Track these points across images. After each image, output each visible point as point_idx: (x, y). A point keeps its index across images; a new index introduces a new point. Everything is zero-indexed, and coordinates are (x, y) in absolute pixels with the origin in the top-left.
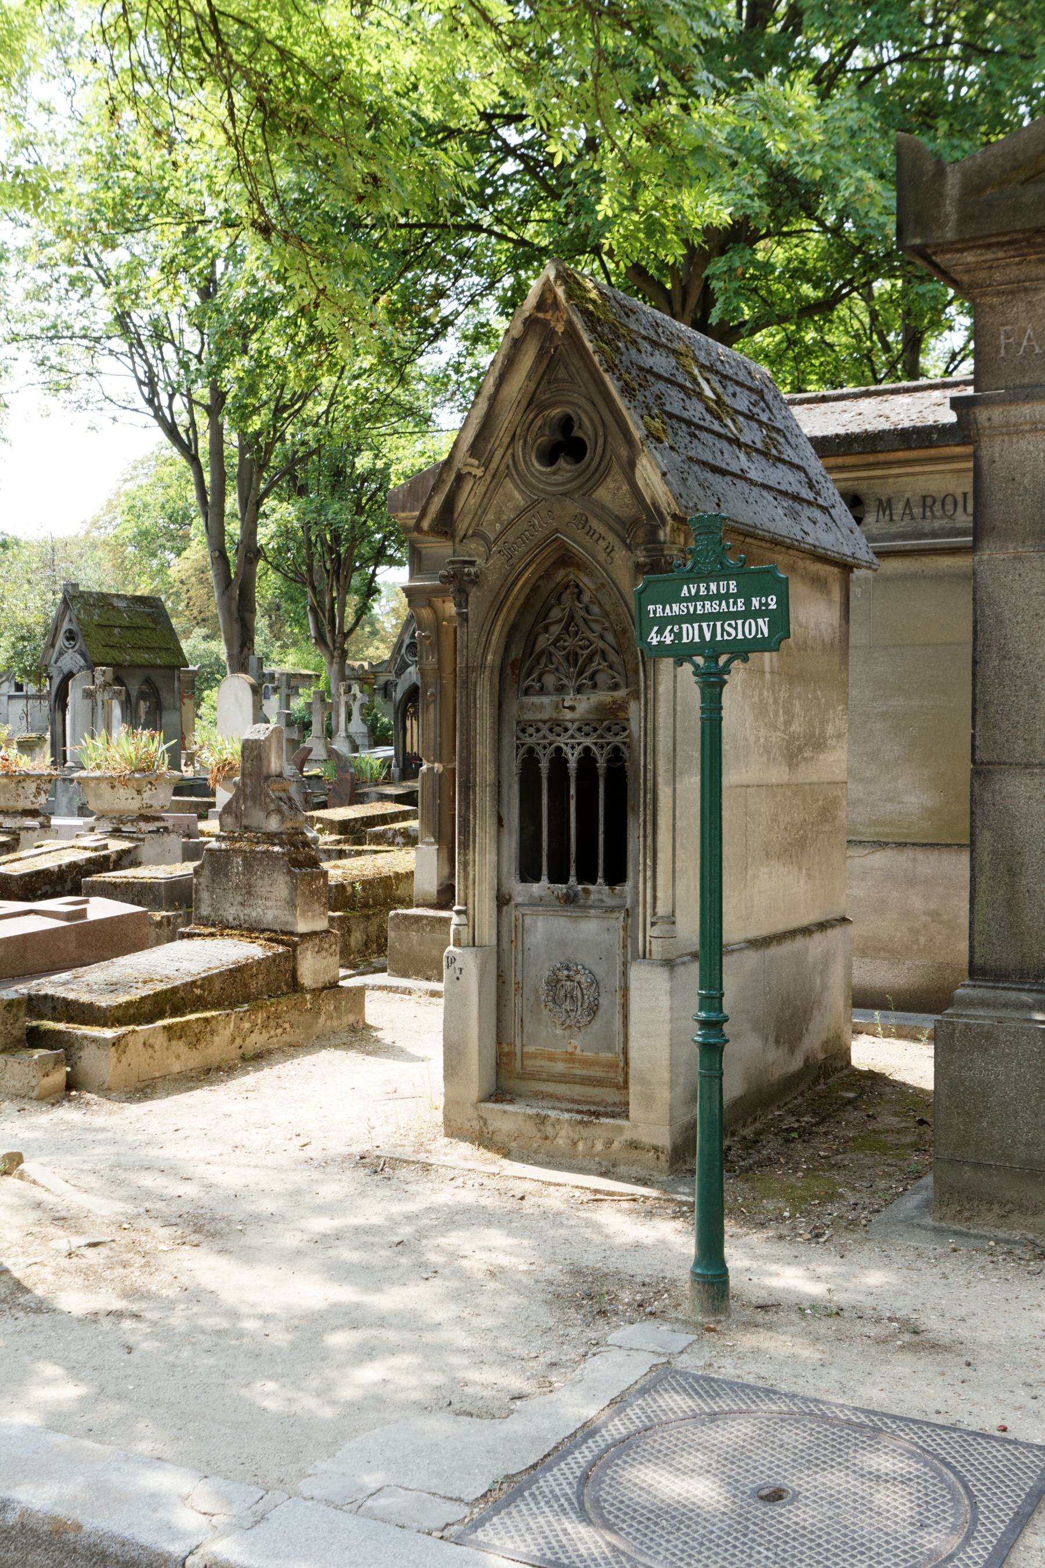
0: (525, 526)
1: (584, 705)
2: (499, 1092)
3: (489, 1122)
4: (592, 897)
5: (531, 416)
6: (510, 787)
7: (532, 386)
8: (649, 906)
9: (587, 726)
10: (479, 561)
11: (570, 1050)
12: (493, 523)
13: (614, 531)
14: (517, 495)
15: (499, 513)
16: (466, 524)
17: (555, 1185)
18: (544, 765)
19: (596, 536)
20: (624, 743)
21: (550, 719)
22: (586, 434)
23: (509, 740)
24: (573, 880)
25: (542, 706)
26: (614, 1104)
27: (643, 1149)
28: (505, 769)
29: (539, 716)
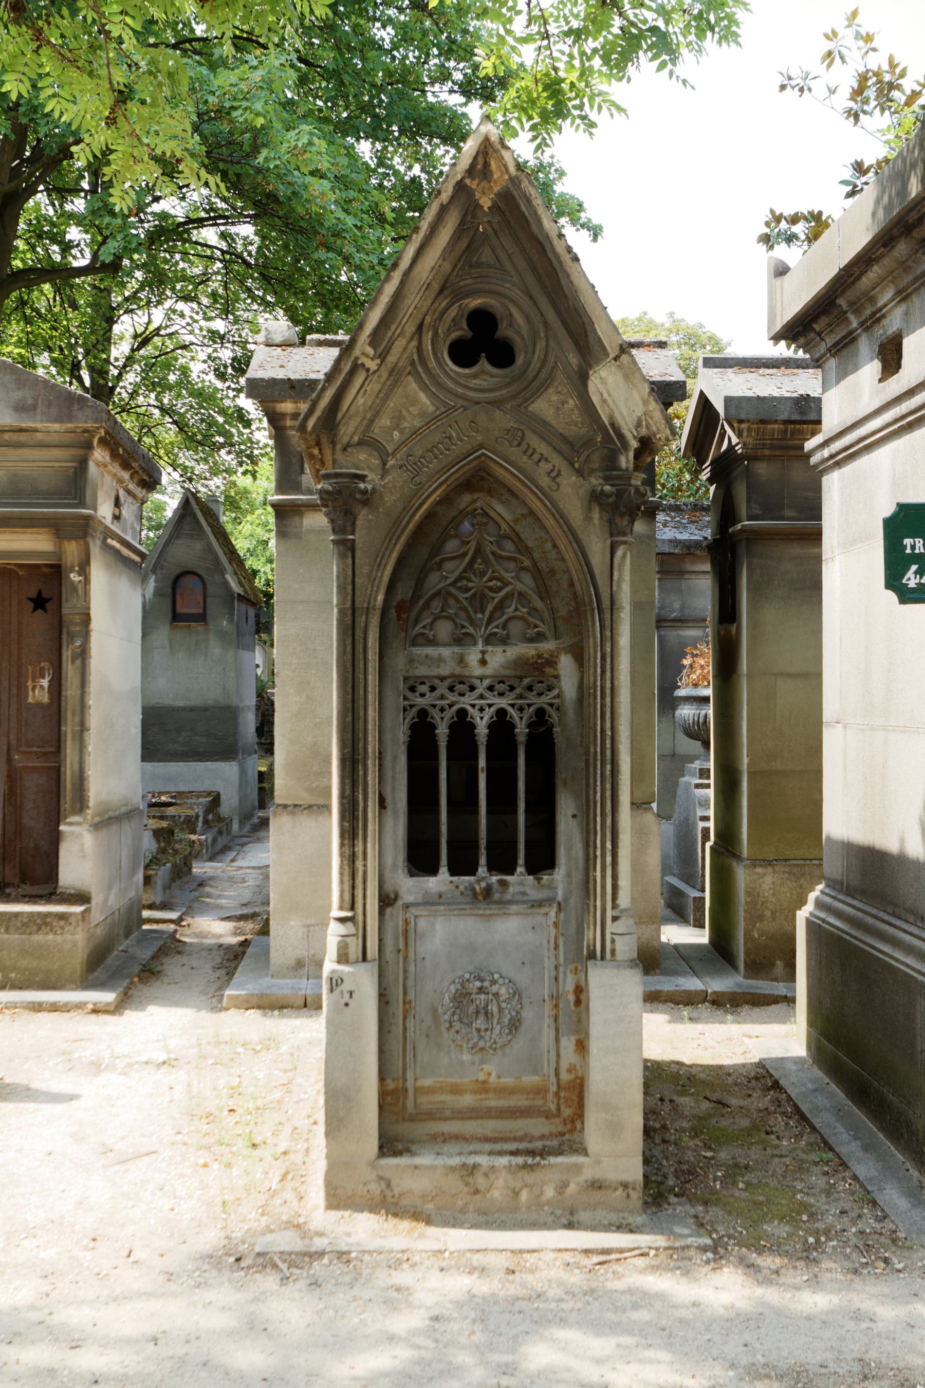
0: (438, 437)
1: (499, 659)
2: (390, 1145)
3: (394, 1183)
4: (511, 890)
5: (444, 304)
6: (395, 758)
7: (447, 267)
10: (371, 476)
11: (482, 1077)
12: (389, 430)
13: (560, 453)
14: (423, 397)
16: (351, 429)
17: (529, 1251)
18: (442, 731)
19: (536, 457)
20: (551, 705)
21: (452, 675)
22: (519, 333)
23: (394, 701)
24: (482, 871)
25: (440, 660)
26: (542, 1137)
27: (608, 1187)
28: (388, 737)
29: (436, 672)
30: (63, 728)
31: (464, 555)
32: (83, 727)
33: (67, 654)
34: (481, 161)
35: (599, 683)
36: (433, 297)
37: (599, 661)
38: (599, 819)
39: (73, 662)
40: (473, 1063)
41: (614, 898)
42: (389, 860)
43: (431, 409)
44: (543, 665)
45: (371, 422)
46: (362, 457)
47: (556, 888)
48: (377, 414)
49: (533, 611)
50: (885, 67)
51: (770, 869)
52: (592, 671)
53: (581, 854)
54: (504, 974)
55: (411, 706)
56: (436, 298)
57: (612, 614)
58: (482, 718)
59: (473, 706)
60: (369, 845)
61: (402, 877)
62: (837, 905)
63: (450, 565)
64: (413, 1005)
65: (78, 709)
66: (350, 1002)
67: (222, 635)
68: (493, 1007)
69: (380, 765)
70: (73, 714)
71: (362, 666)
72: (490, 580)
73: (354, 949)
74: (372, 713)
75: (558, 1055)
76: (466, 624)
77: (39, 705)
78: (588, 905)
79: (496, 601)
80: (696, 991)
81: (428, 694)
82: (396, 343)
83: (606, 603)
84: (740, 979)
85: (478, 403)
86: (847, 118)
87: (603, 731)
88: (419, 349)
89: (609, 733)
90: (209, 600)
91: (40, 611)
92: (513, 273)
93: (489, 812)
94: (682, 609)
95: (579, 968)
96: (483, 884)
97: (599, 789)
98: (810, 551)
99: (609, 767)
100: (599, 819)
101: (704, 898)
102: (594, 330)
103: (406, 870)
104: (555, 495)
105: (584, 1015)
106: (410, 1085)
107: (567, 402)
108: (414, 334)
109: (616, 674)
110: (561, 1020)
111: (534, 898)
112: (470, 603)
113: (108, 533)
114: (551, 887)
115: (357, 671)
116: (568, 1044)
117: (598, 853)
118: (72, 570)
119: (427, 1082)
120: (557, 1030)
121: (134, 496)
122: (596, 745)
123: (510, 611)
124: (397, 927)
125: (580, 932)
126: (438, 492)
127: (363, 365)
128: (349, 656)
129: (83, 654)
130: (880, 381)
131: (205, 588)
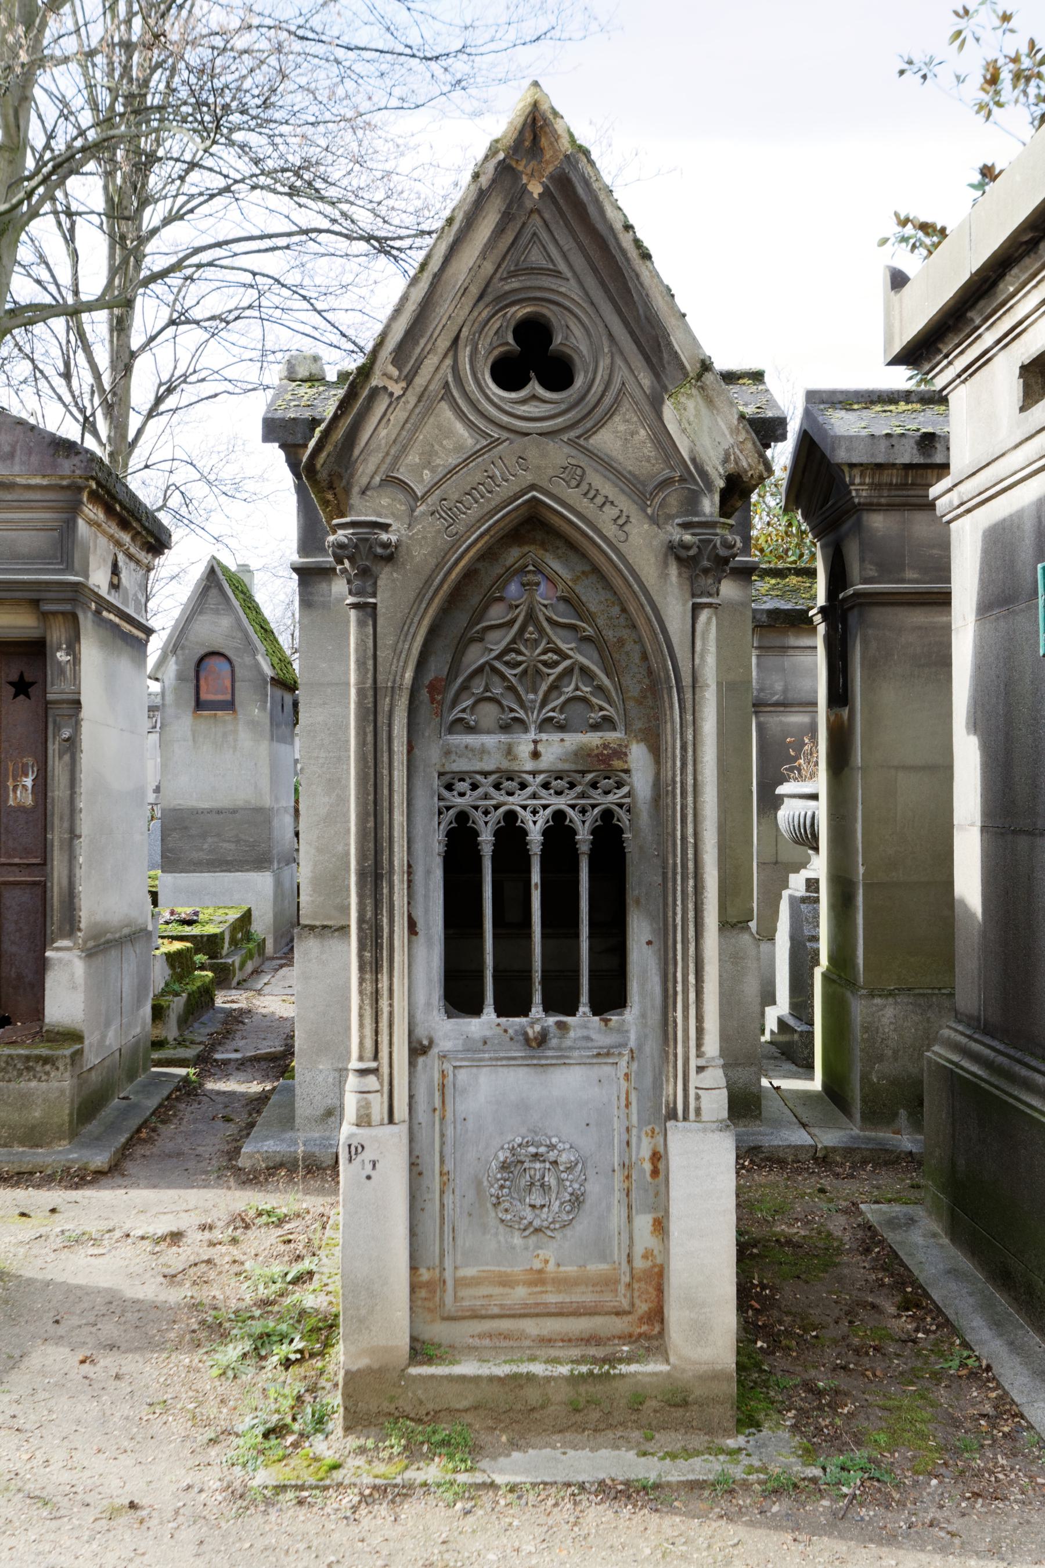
0: (479, 477)
1: (556, 749)
4: (572, 1034)
6: (428, 872)
8: (692, 1043)
9: (557, 780)
11: (537, 1265)
12: (417, 470)
14: (460, 428)
15: (429, 455)
16: (371, 467)
18: (486, 838)
19: (599, 500)
20: (621, 806)
21: (498, 771)
23: (426, 802)
24: (537, 1010)
25: (483, 751)
28: (419, 846)
29: (478, 766)
30: (49, 836)
31: (511, 623)
32: (73, 835)
33: (53, 748)
34: (528, 136)
35: (678, 779)
36: (471, 304)
37: (678, 752)
38: (679, 946)
39: (60, 758)
40: (526, 1248)
41: (699, 1045)
42: (421, 998)
43: (470, 442)
44: (609, 757)
45: (397, 458)
46: (385, 501)
47: (627, 1031)
48: (404, 449)
49: (600, 689)
50: (1024, 49)
51: (891, 1000)
52: (669, 764)
53: (658, 990)
54: (564, 1139)
55: (448, 808)
56: (475, 305)
57: (694, 694)
58: (535, 823)
59: (524, 807)
60: (395, 980)
61: (437, 1019)
62: (976, 1047)
63: (492, 636)
64: (452, 1176)
65: (67, 812)
66: (373, 1174)
67: (253, 724)
68: (550, 1179)
69: (409, 881)
70: (61, 819)
71: (386, 759)
72: (544, 653)
73: (378, 1107)
74: (399, 818)
75: (631, 1238)
76: (515, 707)
77: (21, 809)
78: (667, 1053)
79: (552, 678)
80: (802, 1146)
81: (469, 792)
82: (426, 362)
83: (687, 680)
84: (856, 1131)
85: (527, 434)
86: (978, 112)
87: (684, 838)
88: (455, 369)
89: (691, 840)
90: (237, 684)
91: (22, 697)
92: (569, 275)
93: (544, 936)
94: (785, 691)
95: (657, 1130)
96: (537, 1028)
97: (679, 909)
98: (936, 619)
99: (691, 882)
100: (679, 946)
101: (812, 1033)
102: (669, 344)
103: (443, 1010)
104: (622, 547)
105: (663, 1188)
106: (448, 1275)
107: (637, 433)
108: (449, 350)
109: (699, 767)
110: (633, 1194)
111: (600, 1044)
112: (520, 680)
113: (104, 604)
114: (622, 1030)
115: (380, 765)
116: (643, 1222)
117: (679, 988)
118: (59, 649)
119: (469, 1272)
120: (630, 1207)
121: (138, 562)
122: (675, 855)
123: (569, 690)
124: (432, 1081)
125: (658, 1086)
126: (479, 545)
127: (385, 388)
128: (370, 747)
129: (72, 745)
130: (1022, 409)
131: (233, 672)
